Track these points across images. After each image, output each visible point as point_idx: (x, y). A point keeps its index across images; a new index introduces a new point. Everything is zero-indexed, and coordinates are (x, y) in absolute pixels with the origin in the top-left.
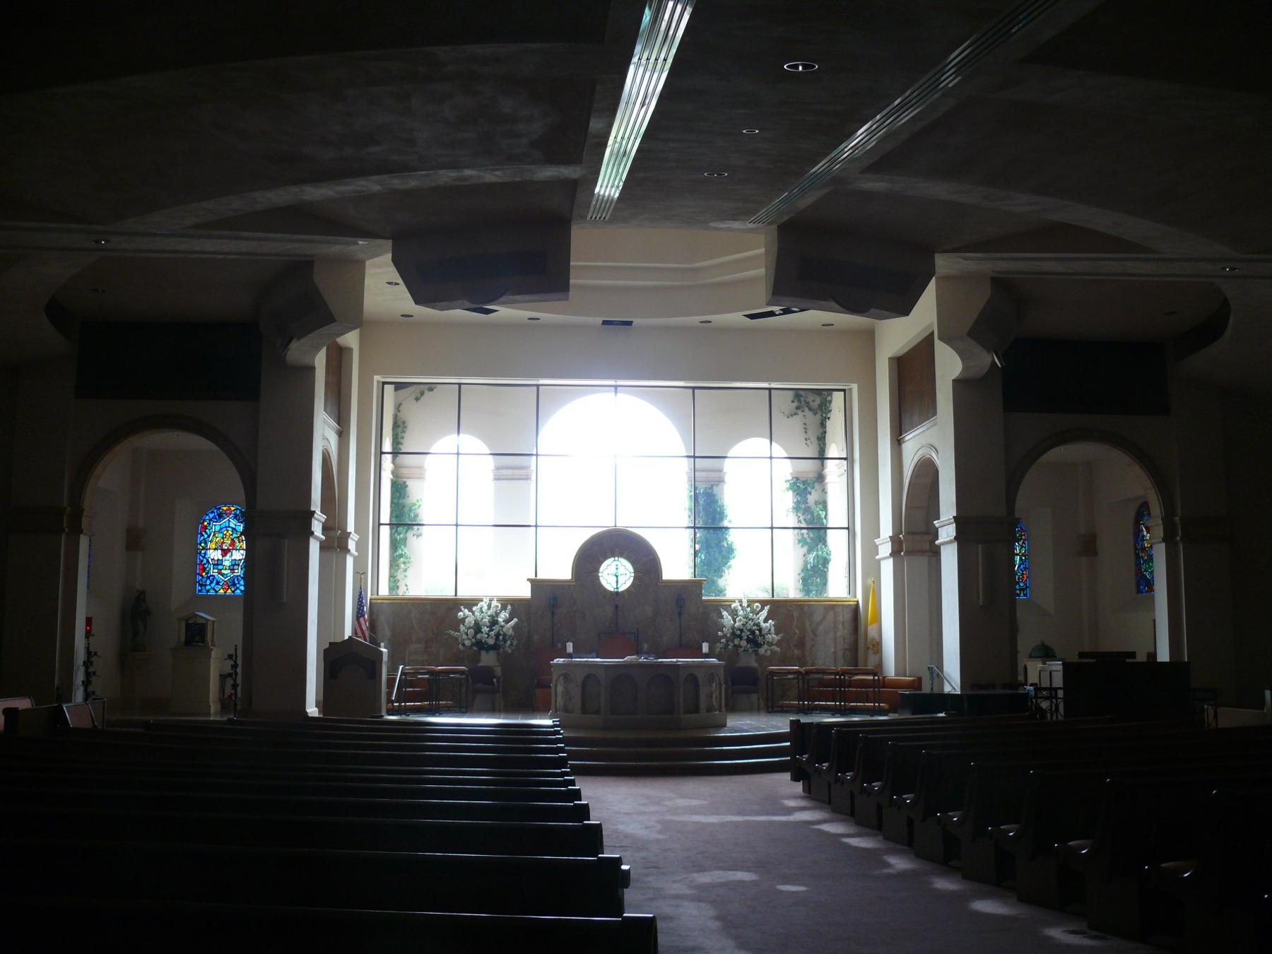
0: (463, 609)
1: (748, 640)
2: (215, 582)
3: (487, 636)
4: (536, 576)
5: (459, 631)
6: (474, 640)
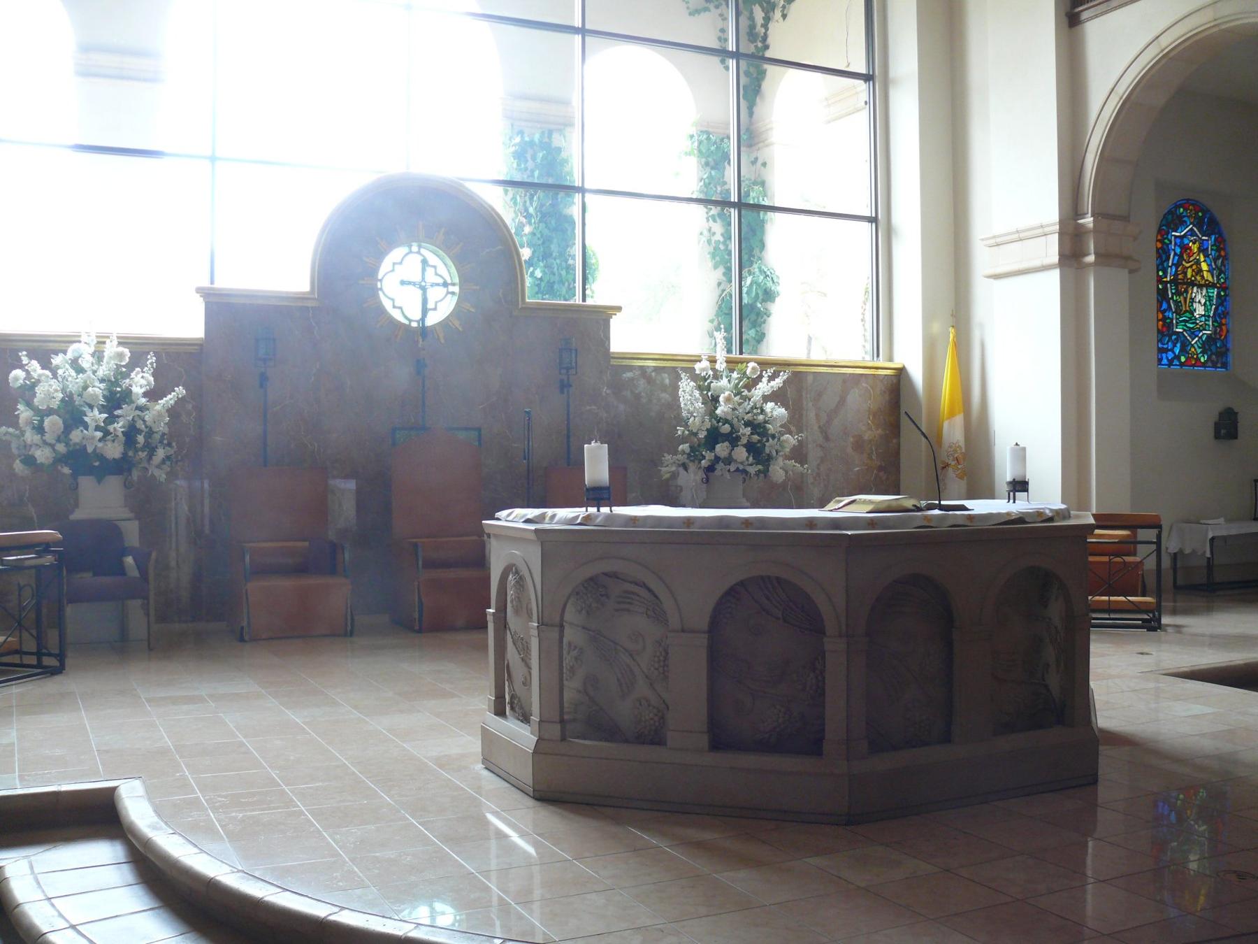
0: (25, 360)
1: (750, 447)
3: (99, 434)
4: (212, 283)
5: (13, 421)
6: (61, 448)
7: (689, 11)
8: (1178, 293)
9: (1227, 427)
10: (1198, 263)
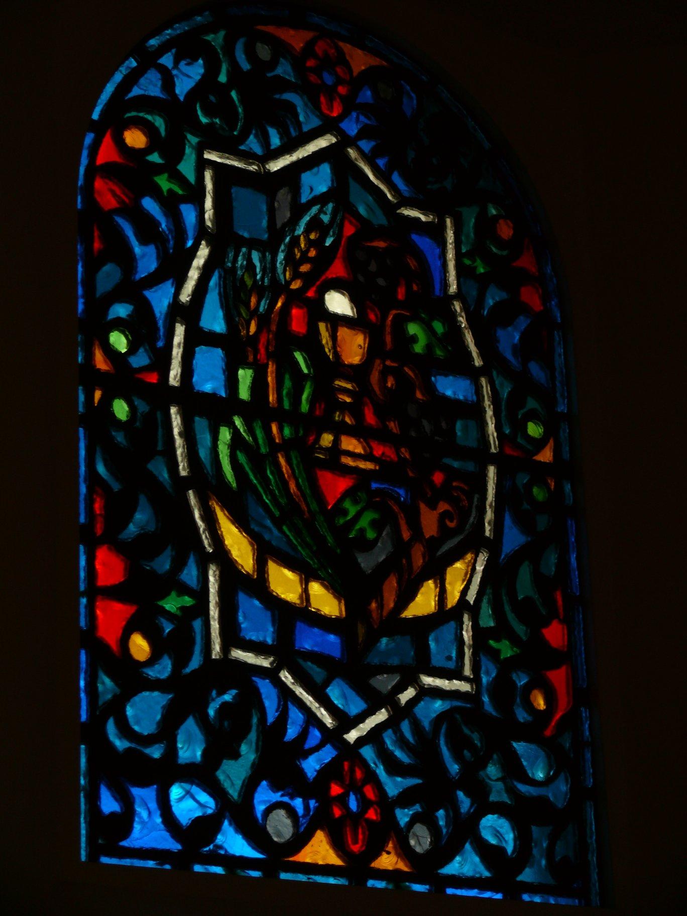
2: (248, 752)
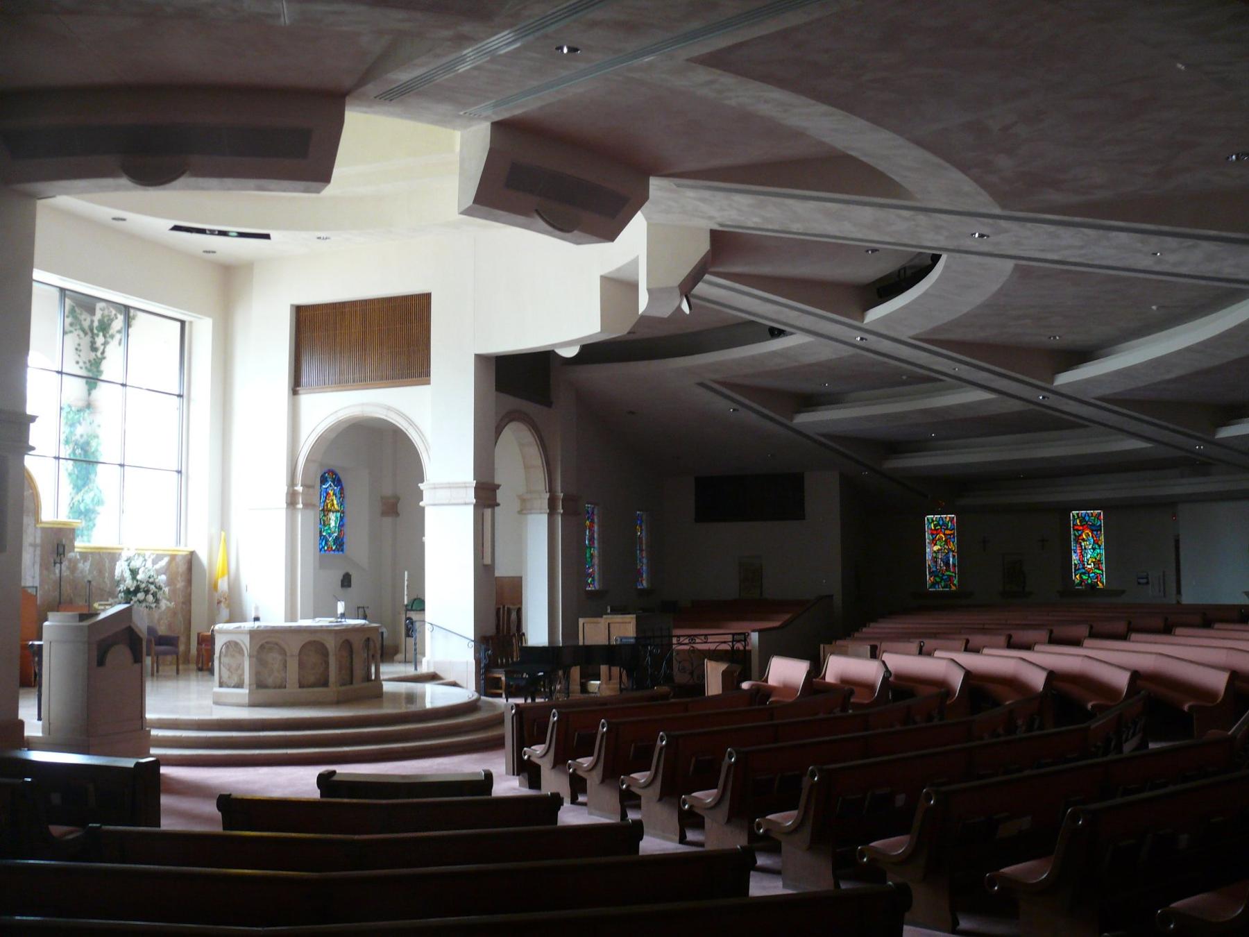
1: (154, 595)
7: (77, 347)
8: (324, 515)
9: (346, 581)
10: (332, 500)
